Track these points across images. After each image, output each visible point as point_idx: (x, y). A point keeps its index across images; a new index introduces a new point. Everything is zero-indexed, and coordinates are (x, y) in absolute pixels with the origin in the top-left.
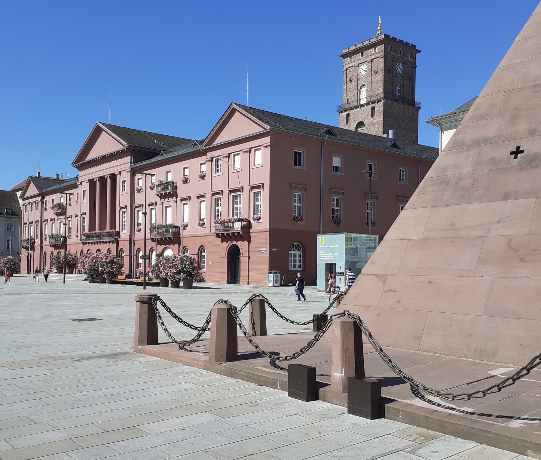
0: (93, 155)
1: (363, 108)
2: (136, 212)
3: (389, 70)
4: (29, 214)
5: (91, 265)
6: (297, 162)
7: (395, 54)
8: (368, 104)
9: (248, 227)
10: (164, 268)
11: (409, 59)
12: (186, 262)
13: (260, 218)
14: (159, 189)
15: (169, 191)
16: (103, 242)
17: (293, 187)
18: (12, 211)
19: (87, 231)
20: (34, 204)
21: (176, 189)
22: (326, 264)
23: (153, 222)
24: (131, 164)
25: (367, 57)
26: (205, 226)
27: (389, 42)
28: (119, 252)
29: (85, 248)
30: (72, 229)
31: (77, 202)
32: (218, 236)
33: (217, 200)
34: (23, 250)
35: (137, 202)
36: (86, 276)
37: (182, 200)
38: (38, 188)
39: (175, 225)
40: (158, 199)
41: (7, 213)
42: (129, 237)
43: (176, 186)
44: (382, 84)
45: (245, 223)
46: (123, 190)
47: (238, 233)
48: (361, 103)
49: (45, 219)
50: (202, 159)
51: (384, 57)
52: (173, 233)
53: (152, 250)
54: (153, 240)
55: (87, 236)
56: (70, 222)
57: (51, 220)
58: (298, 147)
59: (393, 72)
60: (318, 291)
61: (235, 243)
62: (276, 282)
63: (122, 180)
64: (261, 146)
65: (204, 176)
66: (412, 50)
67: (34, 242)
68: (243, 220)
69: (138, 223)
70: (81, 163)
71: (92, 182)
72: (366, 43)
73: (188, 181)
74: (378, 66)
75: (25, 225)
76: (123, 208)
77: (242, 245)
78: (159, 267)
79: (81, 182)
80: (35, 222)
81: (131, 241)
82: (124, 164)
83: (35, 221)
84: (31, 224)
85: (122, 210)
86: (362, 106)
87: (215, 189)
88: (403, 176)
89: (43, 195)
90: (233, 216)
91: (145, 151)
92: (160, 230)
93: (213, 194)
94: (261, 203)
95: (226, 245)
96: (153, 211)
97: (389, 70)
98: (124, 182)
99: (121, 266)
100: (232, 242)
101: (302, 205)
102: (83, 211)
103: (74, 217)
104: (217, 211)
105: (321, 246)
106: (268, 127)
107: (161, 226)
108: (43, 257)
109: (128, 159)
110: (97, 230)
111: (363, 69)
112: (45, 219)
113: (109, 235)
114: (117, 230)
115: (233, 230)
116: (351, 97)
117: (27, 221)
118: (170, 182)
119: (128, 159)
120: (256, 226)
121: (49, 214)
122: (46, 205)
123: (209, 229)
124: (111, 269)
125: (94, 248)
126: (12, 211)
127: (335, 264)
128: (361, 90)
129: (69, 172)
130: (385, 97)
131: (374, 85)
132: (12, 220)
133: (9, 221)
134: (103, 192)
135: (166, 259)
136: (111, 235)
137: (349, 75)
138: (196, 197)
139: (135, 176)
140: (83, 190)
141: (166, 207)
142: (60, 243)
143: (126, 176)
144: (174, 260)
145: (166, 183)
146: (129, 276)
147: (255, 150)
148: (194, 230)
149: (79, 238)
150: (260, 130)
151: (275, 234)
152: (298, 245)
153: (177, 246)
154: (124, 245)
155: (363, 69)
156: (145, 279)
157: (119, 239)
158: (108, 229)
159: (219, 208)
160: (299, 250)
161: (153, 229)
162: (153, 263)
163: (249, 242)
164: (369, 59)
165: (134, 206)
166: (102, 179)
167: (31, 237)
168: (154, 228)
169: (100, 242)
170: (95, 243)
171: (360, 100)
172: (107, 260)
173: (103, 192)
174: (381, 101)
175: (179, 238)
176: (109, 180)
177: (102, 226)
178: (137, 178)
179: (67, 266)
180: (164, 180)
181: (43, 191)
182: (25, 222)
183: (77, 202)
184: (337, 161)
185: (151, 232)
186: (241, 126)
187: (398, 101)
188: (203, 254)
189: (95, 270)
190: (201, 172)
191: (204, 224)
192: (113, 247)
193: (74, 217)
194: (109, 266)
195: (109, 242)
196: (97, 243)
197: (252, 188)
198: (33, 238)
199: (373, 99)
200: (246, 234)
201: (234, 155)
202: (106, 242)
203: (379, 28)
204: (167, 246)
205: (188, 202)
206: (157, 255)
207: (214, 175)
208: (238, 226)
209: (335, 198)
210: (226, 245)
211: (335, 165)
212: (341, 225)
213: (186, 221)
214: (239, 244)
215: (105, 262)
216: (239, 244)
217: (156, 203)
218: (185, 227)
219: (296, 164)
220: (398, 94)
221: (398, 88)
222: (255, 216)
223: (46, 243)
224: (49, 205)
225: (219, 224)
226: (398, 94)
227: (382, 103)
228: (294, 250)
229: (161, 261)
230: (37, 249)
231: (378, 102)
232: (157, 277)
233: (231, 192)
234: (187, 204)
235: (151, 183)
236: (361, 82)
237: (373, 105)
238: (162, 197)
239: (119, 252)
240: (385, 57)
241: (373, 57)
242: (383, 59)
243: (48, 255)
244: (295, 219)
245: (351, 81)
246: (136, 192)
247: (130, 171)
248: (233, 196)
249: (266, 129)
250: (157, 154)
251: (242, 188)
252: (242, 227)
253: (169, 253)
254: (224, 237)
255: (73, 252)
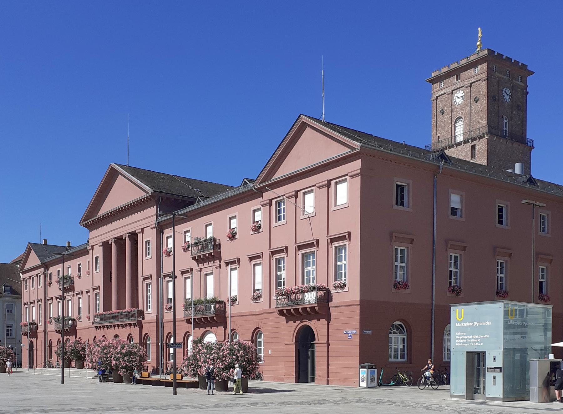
0: (107, 207)
1: (460, 148)
2: (165, 283)
3: (494, 97)
4: (31, 292)
5: (100, 358)
6: (400, 201)
7: (502, 76)
8: (466, 142)
9: (326, 298)
10: (205, 362)
11: (518, 82)
12: (239, 351)
13: (345, 285)
14: (195, 250)
15: (208, 253)
16: (107, 327)
17: (394, 237)
18: (11, 289)
19: (101, 311)
20: (35, 278)
21: (220, 249)
22: (467, 353)
23: (188, 296)
24: (157, 216)
25: (464, 80)
26: (261, 300)
27: (494, 60)
28: (143, 340)
29: (100, 333)
30: (83, 309)
31: (88, 273)
32: (281, 313)
33: (278, 261)
34: (24, 337)
35: (167, 268)
36: (96, 374)
37: (227, 264)
38: (40, 257)
39: (219, 299)
40: (194, 265)
41: (5, 291)
42: (155, 318)
43: (219, 244)
44: (485, 116)
45: (321, 293)
46: (147, 254)
47: (313, 308)
48: (457, 142)
49: (49, 296)
50: (256, 203)
51: (489, 79)
52: (217, 311)
53: (187, 335)
54: (188, 321)
55: (102, 318)
56: (81, 300)
57: (57, 298)
58: (398, 178)
59: (498, 100)
60: (452, 396)
61: (306, 322)
62: (372, 381)
63: (145, 240)
64: (347, 175)
65: (260, 227)
66: (523, 71)
67: (37, 328)
68: (319, 289)
69: (168, 299)
70: (92, 221)
71: (106, 246)
72: (463, 62)
73: (236, 237)
74: (479, 92)
75: (26, 306)
76: (148, 278)
77: (318, 326)
78: (196, 360)
79: (93, 247)
80: (38, 302)
81: (160, 324)
82: (148, 217)
83: (37, 300)
84: (32, 305)
85: (147, 281)
86: (459, 144)
87: (276, 245)
88: (544, 224)
89: (46, 266)
90: (303, 283)
91: (175, 201)
92: (198, 308)
93: (273, 253)
94: (345, 262)
95: (293, 327)
96: (188, 281)
97: (493, 98)
98: (148, 242)
99: (143, 358)
100: (302, 322)
101: (407, 264)
102: (96, 285)
103: (84, 292)
104: (278, 277)
105: (458, 325)
106: (357, 145)
107: (199, 301)
108: (48, 345)
109: (153, 210)
110: (114, 309)
111: (459, 98)
112: (49, 296)
113: (129, 315)
114: (140, 308)
115: (304, 304)
116: (443, 134)
117: (28, 301)
118: (211, 239)
119: (153, 210)
120: (338, 297)
121: (55, 290)
122: (50, 279)
123: (270, 302)
124: (129, 362)
125: (110, 333)
126: (11, 289)
127: (484, 353)
128: (457, 125)
129: (76, 236)
130: (490, 132)
131: (474, 117)
132: (11, 299)
133: (9, 301)
134: (121, 256)
135: (207, 348)
136: (133, 316)
137: (440, 106)
138: (248, 259)
139: (163, 233)
140: (95, 256)
141: (206, 275)
142: (68, 328)
143: (150, 235)
144: (219, 349)
145: (205, 241)
146: (156, 372)
147: (336, 184)
148: (246, 305)
149: (91, 321)
150: (344, 151)
151: (369, 309)
152: (400, 325)
153: (221, 328)
154: (150, 329)
155: (459, 98)
156: (175, 376)
157: (143, 321)
158: (128, 308)
159: (282, 273)
160: (401, 333)
161: (187, 305)
162: (190, 354)
163: (329, 320)
164: (467, 83)
165: (162, 276)
166: (120, 241)
167: (33, 320)
168: (190, 305)
169: (118, 326)
170: (111, 326)
171: (455, 137)
172: (124, 351)
173: (121, 256)
174: (483, 137)
175: (225, 318)
176: (128, 241)
177: (121, 304)
178: (165, 236)
179: (74, 357)
180: (202, 237)
181: (46, 260)
182: (25, 302)
183: (88, 273)
184: (455, 200)
185: (186, 309)
186: (315, 147)
187: (505, 138)
188: (259, 340)
189: (107, 365)
190: (254, 222)
191: (260, 297)
192: (135, 331)
193: (84, 292)
194: (126, 358)
195: (130, 325)
196: (114, 326)
197: (332, 240)
198: (36, 322)
199: (473, 135)
200: (323, 309)
201: (304, 194)
202: (126, 325)
203: (478, 43)
204: (208, 329)
205: (236, 266)
206: (194, 342)
207: (274, 224)
208: (310, 298)
209: (453, 255)
210: (293, 327)
211: (453, 205)
212: (462, 295)
213: (234, 293)
214: (313, 324)
215: (120, 353)
216: (313, 324)
217: (192, 270)
218: (234, 301)
219: (397, 204)
220: (505, 129)
221: (505, 121)
222: (337, 283)
223: (51, 327)
224: (55, 278)
225: (284, 295)
226: (505, 129)
227: (485, 140)
228: (394, 333)
229: (200, 350)
230: (41, 336)
231: (480, 138)
232: (195, 375)
233: (300, 247)
234: (235, 269)
235: (185, 242)
236: (457, 114)
237: (473, 143)
238: (199, 260)
239: (143, 340)
240: (489, 79)
241: (473, 80)
242: (485, 83)
243: (55, 343)
244: (397, 285)
245: (442, 113)
246: (164, 255)
247: (156, 227)
248: (303, 254)
249: (353, 148)
250: (192, 203)
251: (317, 241)
252: (318, 299)
253: (211, 338)
254: (289, 315)
255: (84, 340)
